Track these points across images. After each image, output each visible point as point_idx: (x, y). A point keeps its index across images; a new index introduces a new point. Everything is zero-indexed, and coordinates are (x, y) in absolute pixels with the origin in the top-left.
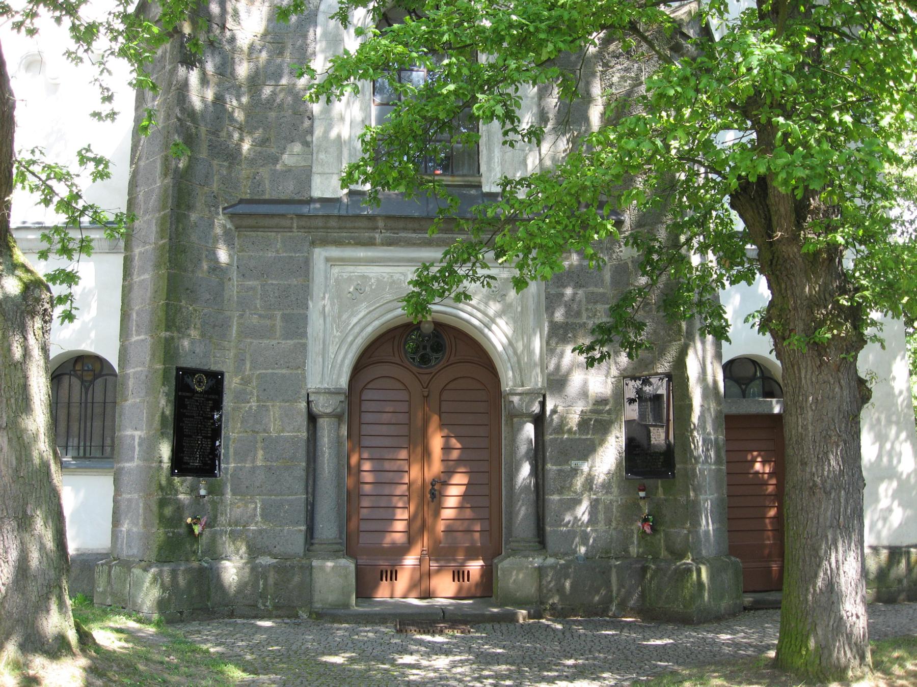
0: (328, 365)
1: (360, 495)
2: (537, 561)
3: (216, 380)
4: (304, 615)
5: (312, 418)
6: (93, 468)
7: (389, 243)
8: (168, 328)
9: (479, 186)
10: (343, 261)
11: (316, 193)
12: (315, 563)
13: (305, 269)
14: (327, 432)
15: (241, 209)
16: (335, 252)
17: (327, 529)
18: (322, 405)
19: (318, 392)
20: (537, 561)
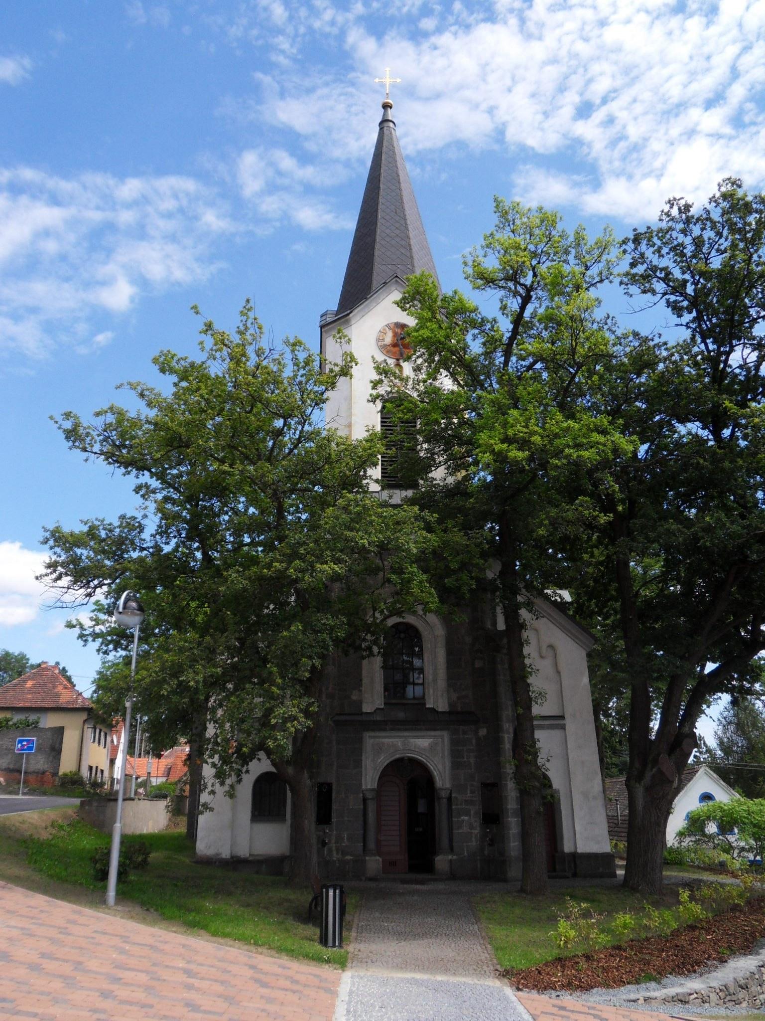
0: (370, 780)
1: (187, 497)
2: (450, 857)
3: (330, 785)
4: (363, 878)
5: (365, 800)
6: (577, 637)
7: (392, 730)
8: (749, 903)
9: (425, 704)
10: (374, 737)
11: (364, 710)
12: (367, 858)
13: (360, 741)
14: (372, 807)
15: (337, 718)
16: (372, 734)
17: (372, 845)
18: (369, 795)
19: (367, 790)
20: (450, 857)
